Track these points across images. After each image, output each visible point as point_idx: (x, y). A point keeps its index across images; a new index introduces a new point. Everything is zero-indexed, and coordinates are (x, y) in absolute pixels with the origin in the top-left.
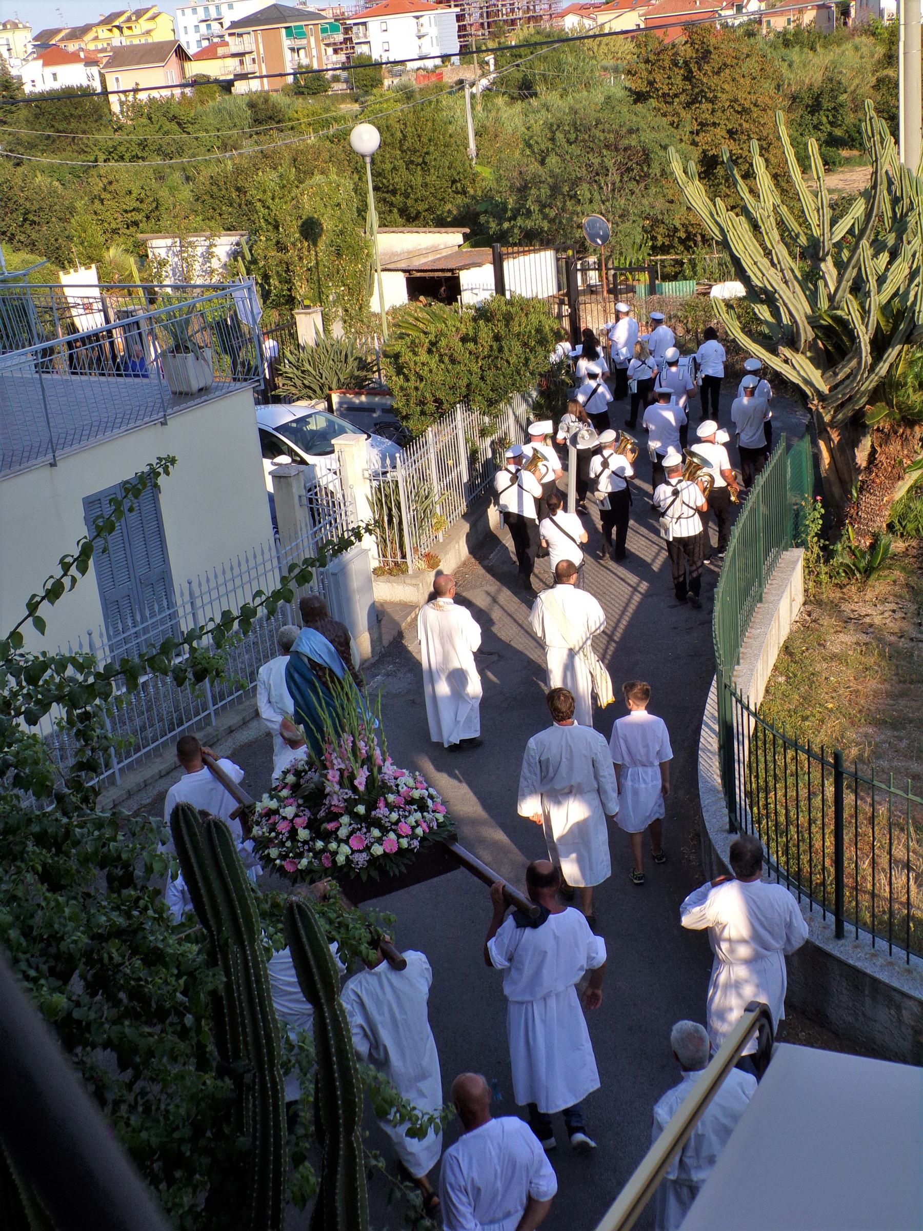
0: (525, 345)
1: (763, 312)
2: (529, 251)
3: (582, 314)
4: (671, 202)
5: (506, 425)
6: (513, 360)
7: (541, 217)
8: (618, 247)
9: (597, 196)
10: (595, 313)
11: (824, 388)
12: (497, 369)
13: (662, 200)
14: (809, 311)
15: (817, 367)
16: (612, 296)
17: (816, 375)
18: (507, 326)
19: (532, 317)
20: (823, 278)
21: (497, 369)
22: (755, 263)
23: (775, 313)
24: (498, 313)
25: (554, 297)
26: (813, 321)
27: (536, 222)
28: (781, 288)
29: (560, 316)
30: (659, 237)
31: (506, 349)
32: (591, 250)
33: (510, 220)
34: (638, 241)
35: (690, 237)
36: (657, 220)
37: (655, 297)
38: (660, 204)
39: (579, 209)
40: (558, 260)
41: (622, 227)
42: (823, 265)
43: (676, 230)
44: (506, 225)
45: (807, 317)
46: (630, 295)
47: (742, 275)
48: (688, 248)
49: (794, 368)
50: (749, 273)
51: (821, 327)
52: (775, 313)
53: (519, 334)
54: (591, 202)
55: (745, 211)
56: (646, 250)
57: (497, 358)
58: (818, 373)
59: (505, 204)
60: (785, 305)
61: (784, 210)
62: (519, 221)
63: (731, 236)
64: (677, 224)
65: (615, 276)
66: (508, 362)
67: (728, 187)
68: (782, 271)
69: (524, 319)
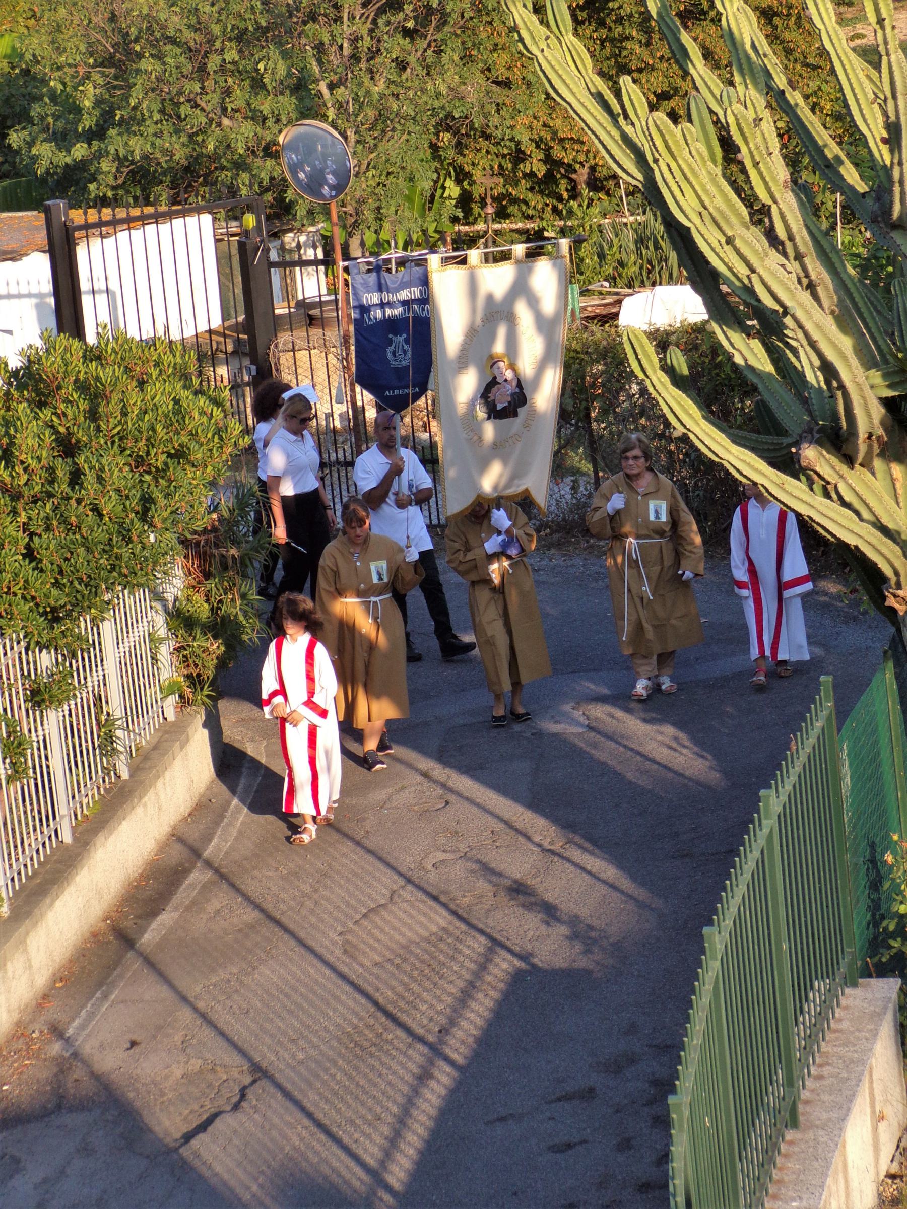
0: (139, 462)
2: (143, 220)
6: (109, 505)
12: (70, 528)
18: (93, 415)
28: (799, 302)
30: (477, 174)
31: (90, 478)
44: (80, 151)
47: (703, 277)
62: (116, 141)
66: (96, 510)
68: (799, 257)
69: (134, 398)
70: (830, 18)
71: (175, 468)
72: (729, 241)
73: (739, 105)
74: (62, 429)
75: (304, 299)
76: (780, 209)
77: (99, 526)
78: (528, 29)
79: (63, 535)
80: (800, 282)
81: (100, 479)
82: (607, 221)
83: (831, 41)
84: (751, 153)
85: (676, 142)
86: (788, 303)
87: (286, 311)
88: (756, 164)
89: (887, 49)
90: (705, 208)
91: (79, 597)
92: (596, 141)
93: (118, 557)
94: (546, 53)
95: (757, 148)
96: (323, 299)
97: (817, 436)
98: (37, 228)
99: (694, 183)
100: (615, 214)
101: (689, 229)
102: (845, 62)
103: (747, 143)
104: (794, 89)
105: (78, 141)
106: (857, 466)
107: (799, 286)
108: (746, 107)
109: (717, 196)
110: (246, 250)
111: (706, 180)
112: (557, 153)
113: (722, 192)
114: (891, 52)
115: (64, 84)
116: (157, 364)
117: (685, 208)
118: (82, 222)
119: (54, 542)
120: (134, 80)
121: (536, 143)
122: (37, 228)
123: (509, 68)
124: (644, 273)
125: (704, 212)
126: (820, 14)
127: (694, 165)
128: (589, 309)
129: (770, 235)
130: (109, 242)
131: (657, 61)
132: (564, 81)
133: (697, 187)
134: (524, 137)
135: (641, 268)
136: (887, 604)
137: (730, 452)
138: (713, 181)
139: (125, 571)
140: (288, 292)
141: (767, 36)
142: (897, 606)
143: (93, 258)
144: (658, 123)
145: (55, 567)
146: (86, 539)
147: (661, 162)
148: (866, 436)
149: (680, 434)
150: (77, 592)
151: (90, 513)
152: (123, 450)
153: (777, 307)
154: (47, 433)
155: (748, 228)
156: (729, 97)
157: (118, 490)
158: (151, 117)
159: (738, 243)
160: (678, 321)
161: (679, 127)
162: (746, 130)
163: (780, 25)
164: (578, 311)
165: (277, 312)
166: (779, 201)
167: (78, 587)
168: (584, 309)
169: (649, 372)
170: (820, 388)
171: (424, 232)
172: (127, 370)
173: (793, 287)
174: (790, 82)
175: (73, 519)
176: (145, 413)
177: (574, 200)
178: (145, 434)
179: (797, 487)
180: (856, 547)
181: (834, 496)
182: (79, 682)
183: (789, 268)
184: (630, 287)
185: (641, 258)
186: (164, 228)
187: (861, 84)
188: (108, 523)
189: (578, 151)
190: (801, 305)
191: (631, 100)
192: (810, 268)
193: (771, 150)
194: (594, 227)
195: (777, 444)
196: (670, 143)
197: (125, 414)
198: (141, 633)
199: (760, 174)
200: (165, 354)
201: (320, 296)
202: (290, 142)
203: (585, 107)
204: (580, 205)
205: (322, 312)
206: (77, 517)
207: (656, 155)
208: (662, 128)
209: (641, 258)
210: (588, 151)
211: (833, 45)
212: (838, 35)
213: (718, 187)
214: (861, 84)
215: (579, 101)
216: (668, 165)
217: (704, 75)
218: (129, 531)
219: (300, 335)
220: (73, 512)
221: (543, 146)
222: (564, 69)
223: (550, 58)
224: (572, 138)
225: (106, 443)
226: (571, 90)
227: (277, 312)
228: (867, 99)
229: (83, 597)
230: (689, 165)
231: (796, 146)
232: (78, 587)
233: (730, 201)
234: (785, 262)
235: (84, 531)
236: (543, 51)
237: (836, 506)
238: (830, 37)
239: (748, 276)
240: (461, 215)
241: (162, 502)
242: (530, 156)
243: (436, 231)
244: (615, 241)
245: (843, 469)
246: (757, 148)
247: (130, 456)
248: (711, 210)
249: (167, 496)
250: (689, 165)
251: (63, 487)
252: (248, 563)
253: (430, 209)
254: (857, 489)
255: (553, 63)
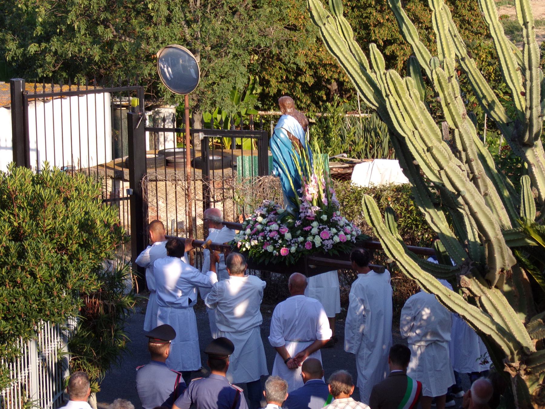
0: (61, 248)
1: (438, 221)
2: (70, 94)
3: (151, 199)
4: (293, 28)
5: (25, 373)
6: (42, 272)
7: (89, 39)
8: (209, 94)
9: (178, 13)
10: (171, 196)
11: (530, 343)
12: (15, 284)
13: (279, 26)
14: (507, 223)
15: (518, 308)
16: (199, 172)
17: (515, 321)
18: (33, 217)
19: (75, 205)
20: (529, 172)
21: (15, 284)
22: (429, 150)
23: (456, 221)
24: (21, 196)
25: (106, 166)
26: (515, 238)
27: (81, 46)
28: (467, 189)
29: (115, 199)
30: (273, 82)
31: (30, 255)
32: (167, 96)
33: (39, 40)
34: (240, 86)
35: (320, 83)
36: (271, 56)
37: (267, 179)
38: (277, 31)
39: (150, 31)
40: (114, 108)
41: (217, 62)
42: (529, 154)
43: (299, 72)
44: (33, 48)
45: (503, 230)
46: (228, 171)
47: (400, 150)
48: (316, 101)
49: (485, 311)
50: (418, 161)
51: (526, 249)
52: (456, 221)
53: (52, 231)
54: (169, 20)
55: (411, 67)
56: (251, 100)
57: (15, 267)
58: (520, 318)
59: (33, 15)
60: (473, 214)
61: (471, 65)
62: (55, 44)
63: (391, 102)
64: (301, 61)
65: (204, 142)
66: (32, 274)
67: (381, 11)
68: (469, 161)
69: (61, 208)
70: (495, 18)
71: (83, 253)
72: (429, 150)
73: (440, 69)
74: (16, 224)
75: (165, 149)
76: (460, 132)
77: (34, 284)
78: (317, 11)
79: (12, 288)
80: (468, 176)
81: (37, 257)
82: (347, 115)
83: (495, 31)
84: (445, 97)
85: (402, 89)
86: (461, 189)
87: (154, 156)
88: (447, 105)
89: (528, 40)
90: (416, 129)
91: (18, 326)
92: (353, 81)
93: (44, 304)
94: (327, 26)
95: (449, 95)
96: (177, 150)
97: (471, 267)
98: (4, 93)
99: (411, 114)
100: (352, 112)
101: (404, 138)
102: (503, 45)
103: (443, 91)
104: (471, 57)
105: (33, 42)
106: (493, 287)
107: (468, 179)
108: (443, 68)
109: (424, 122)
110: (132, 119)
111: (418, 112)
112: (321, 71)
113: (427, 120)
114: (531, 42)
115: (27, 6)
116: (77, 189)
117: (405, 129)
118: (33, 93)
119: (6, 292)
120: (70, 9)
121: (309, 65)
122: (4, 93)
123: (296, 19)
124: (368, 150)
125: (416, 132)
126: (489, 15)
127: (413, 105)
128: (334, 169)
129: (452, 145)
130: (49, 105)
131: (385, 21)
132: (336, 43)
133: (413, 116)
134: (302, 64)
135: (366, 146)
136: (505, 370)
137: (420, 274)
138: (422, 113)
139: (48, 312)
140: (155, 143)
141: (451, 11)
142: (511, 372)
143: (36, 112)
144: (392, 76)
145: (5, 308)
146: (26, 292)
147: (390, 97)
148: (500, 270)
149: (391, 262)
150: (18, 323)
151: (29, 276)
152: (52, 240)
153: (454, 191)
154: (7, 225)
155: (441, 142)
156: (434, 63)
157: (47, 264)
158: (79, 31)
159: (434, 151)
160: (388, 183)
161: (404, 79)
162: (443, 84)
163: (460, 5)
164: (328, 170)
165: (148, 156)
166: (460, 127)
167: (19, 320)
168: (331, 169)
169: (376, 223)
170: (476, 242)
171: (239, 114)
172: (59, 192)
173: (464, 180)
174: (469, 53)
175: (19, 280)
176: (68, 218)
177: (330, 102)
178: (66, 231)
179: (457, 298)
180: (490, 336)
181: (479, 305)
182: (13, 376)
183: (463, 168)
184: (359, 158)
185: (367, 141)
186: (83, 99)
187: (511, 59)
188: (40, 283)
189: (334, 72)
190: (468, 190)
191: (375, 58)
192: (475, 168)
193: (457, 95)
194: (340, 119)
195: (447, 270)
196: (399, 88)
197: (55, 218)
198: (53, 349)
199: (450, 110)
200: (83, 183)
201: (174, 148)
202: (163, 57)
203: (348, 60)
204: (332, 106)
205: (175, 158)
206: (21, 278)
207: (388, 92)
208: (394, 79)
209: (367, 141)
210: (340, 72)
211: (496, 34)
212: (499, 29)
213: (425, 116)
214: (511, 59)
215: (344, 56)
216: (396, 102)
217: (419, 46)
218: (52, 289)
219: (161, 170)
220: (19, 275)
221: (313, 67)
222: (337, 36)
223: (328, 29)
224: (331, 64)
225: (42, 234)
226: (340, 49)
227: (148, 156)
228: (514, 68)
229: (21, 326)
230: (409, 103)
231: (464, 79)
232: (19, 320)
233: (431, 125)
234: (461, 164)
235: (24, 287)
236: (325, 24)
237: (479, 310)
238: (494, 29)
239: (439, 171)
240: (260, 106)
241: (74, 273)
242: (305, 73)
243: (246, 114)
244: (352, 129)
245: (485, 289)
246: (449, 95)
247: (56, 243)
248: (420, 130)
249: (78, 270)
250: (409, 103)
251: (14, 259)
252: (121, 311)
253: (243, 100)
254: (493, 300)
255: (330, 32)
